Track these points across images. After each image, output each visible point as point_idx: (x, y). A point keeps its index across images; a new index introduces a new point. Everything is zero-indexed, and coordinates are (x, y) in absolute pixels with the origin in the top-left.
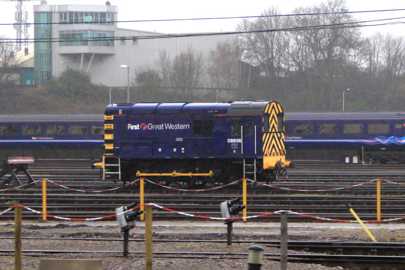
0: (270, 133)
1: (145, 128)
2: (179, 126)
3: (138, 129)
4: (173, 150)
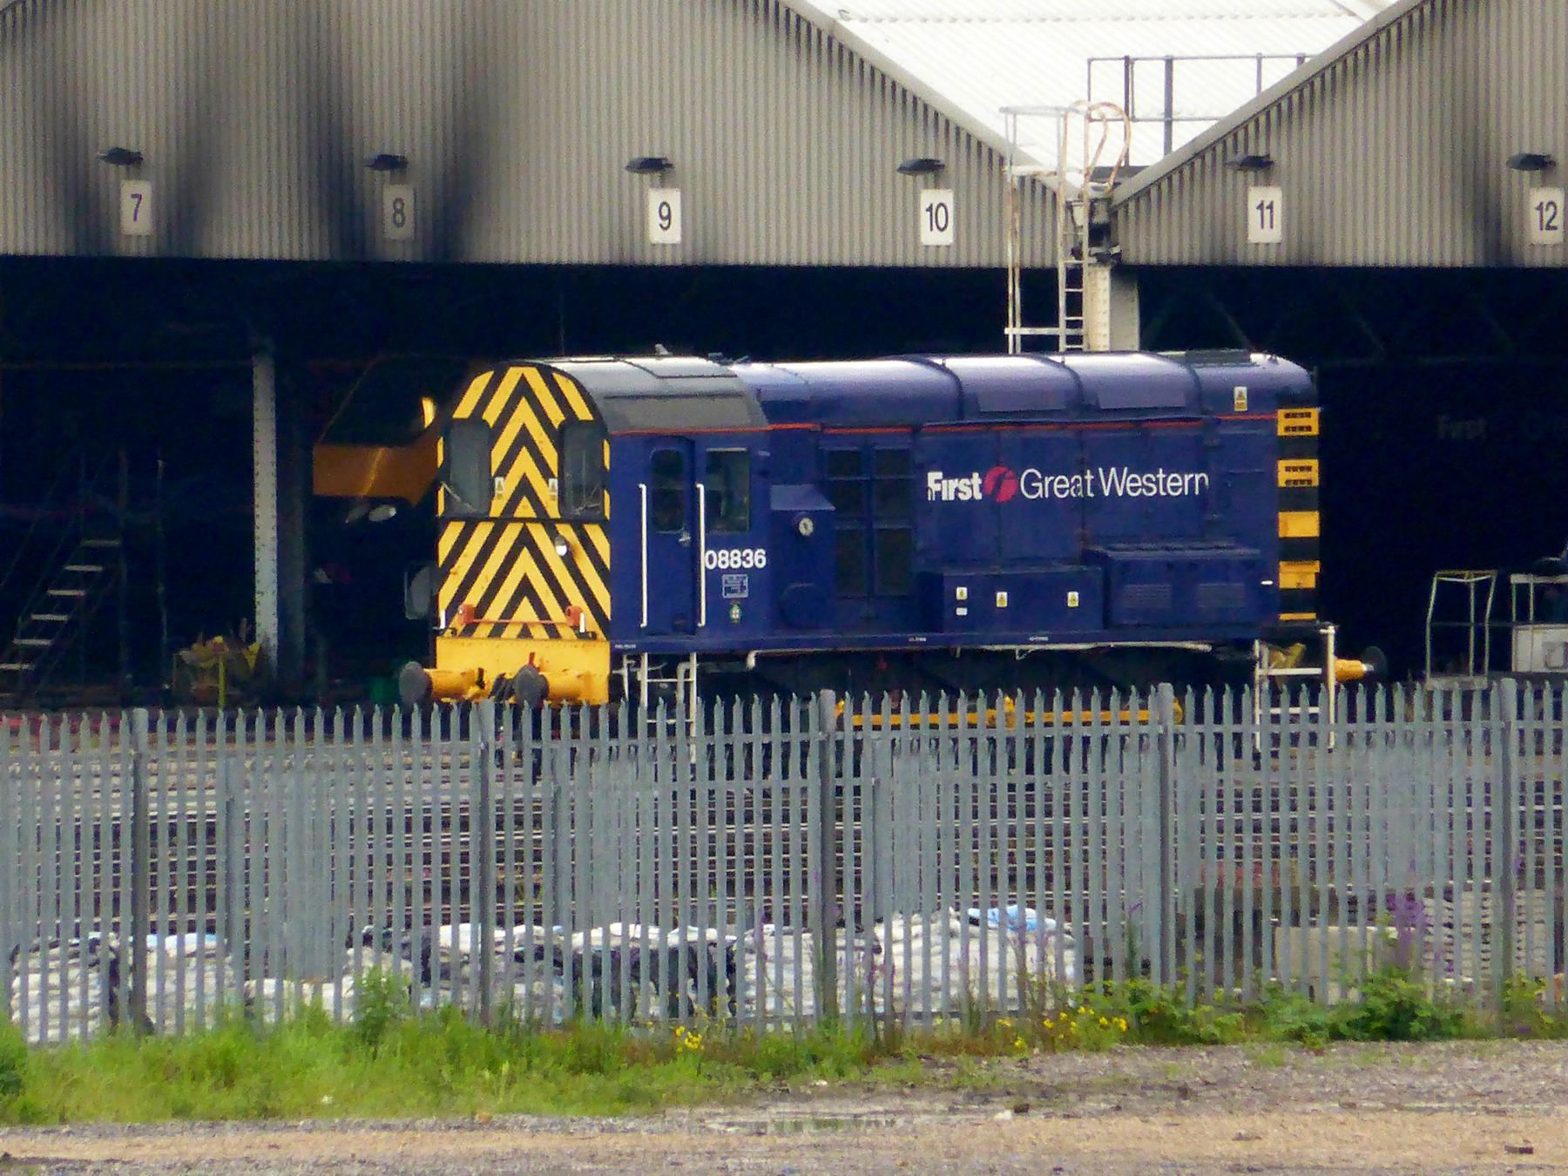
0: (500, 525)
1: (1006, 492)
2: (1165, 480)
3: (978, 496)
4: (1066, 597)
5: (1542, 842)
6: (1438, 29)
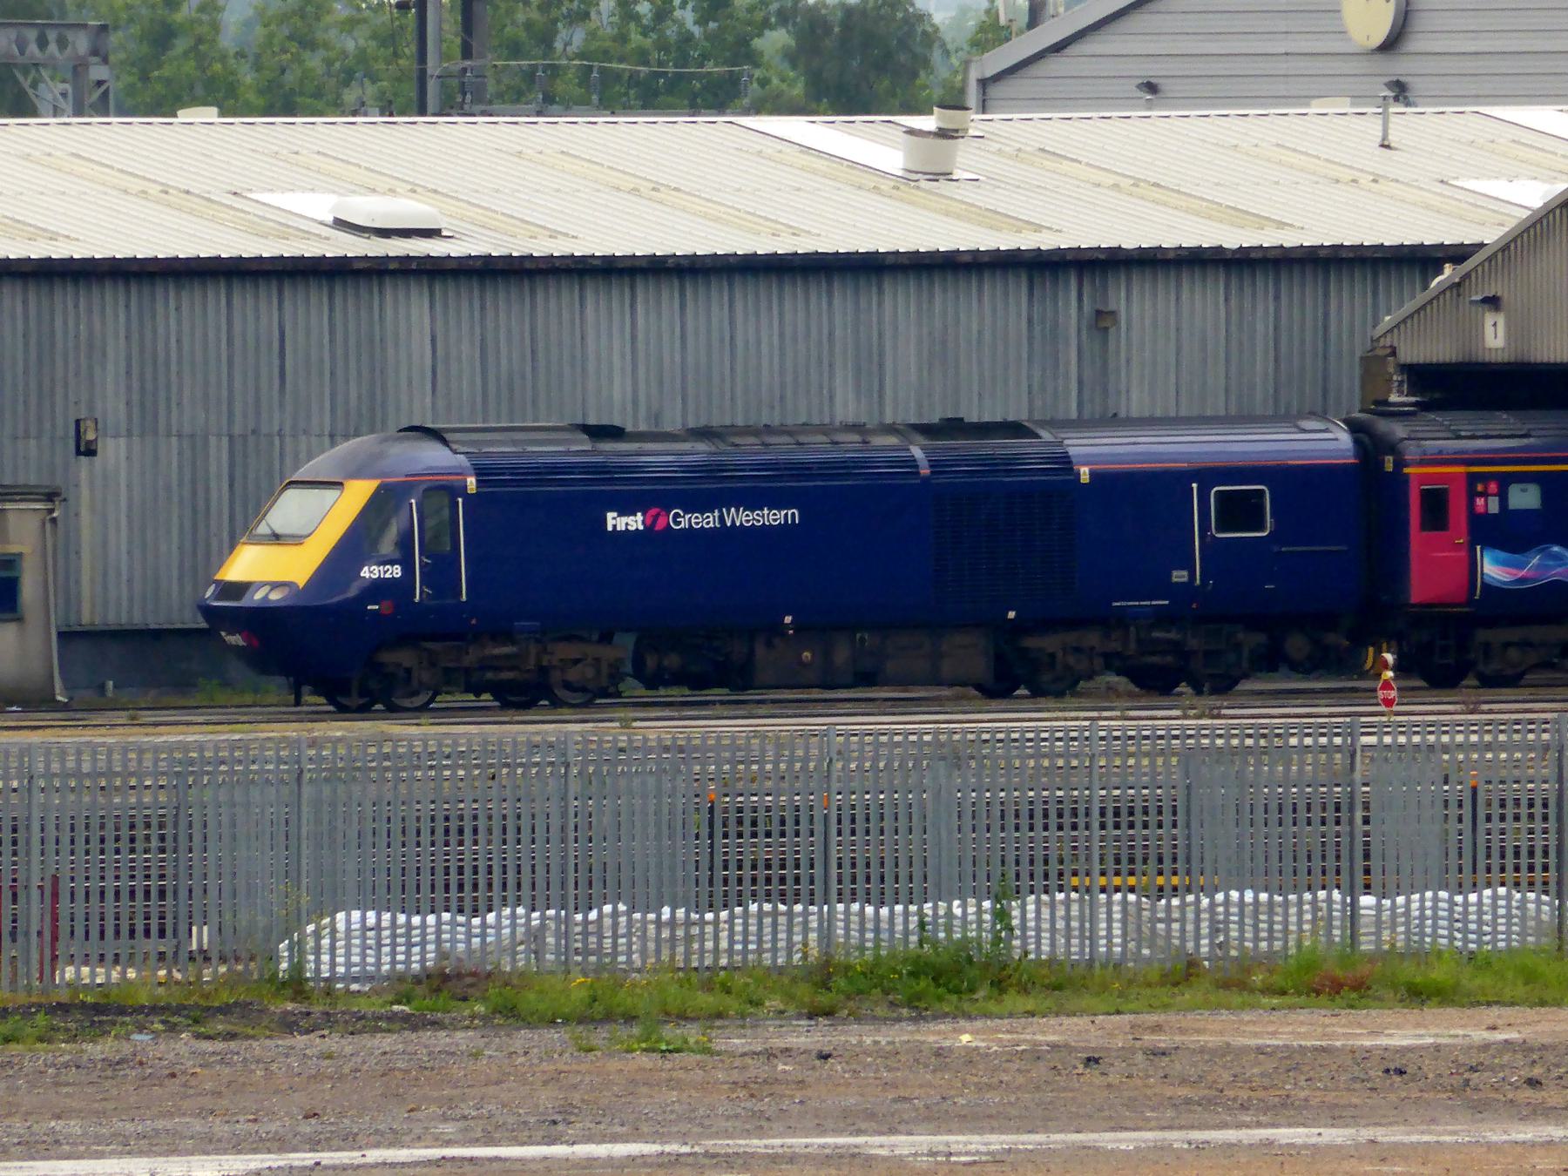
1: (660, 525)
3: (641, 527)
5: (160, 918)
6: (1532, 252)
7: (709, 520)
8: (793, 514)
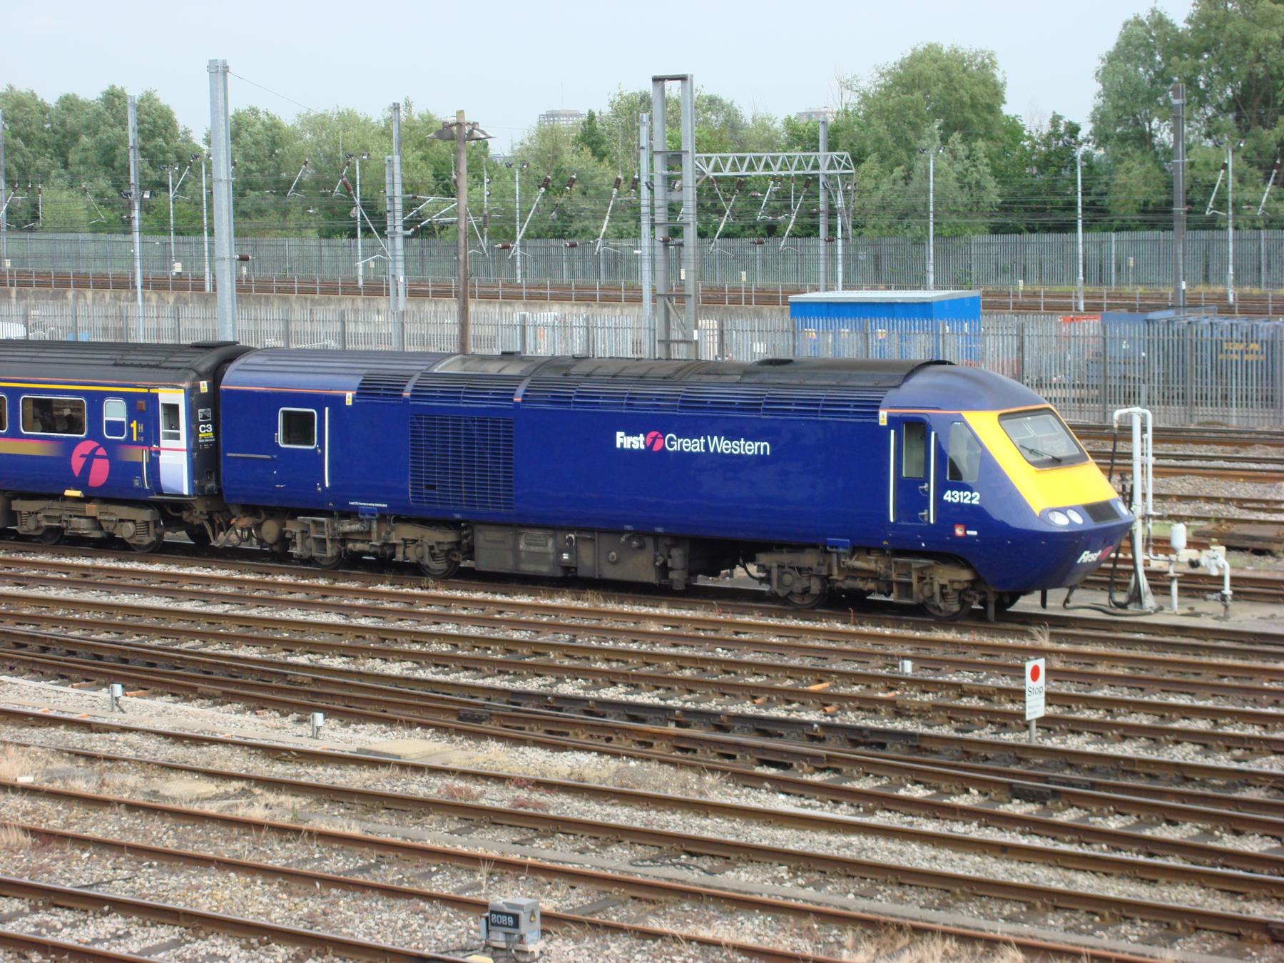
1: (657, 447)
3: (643, 447)
7: (693, 445)
8: (765, 447)
